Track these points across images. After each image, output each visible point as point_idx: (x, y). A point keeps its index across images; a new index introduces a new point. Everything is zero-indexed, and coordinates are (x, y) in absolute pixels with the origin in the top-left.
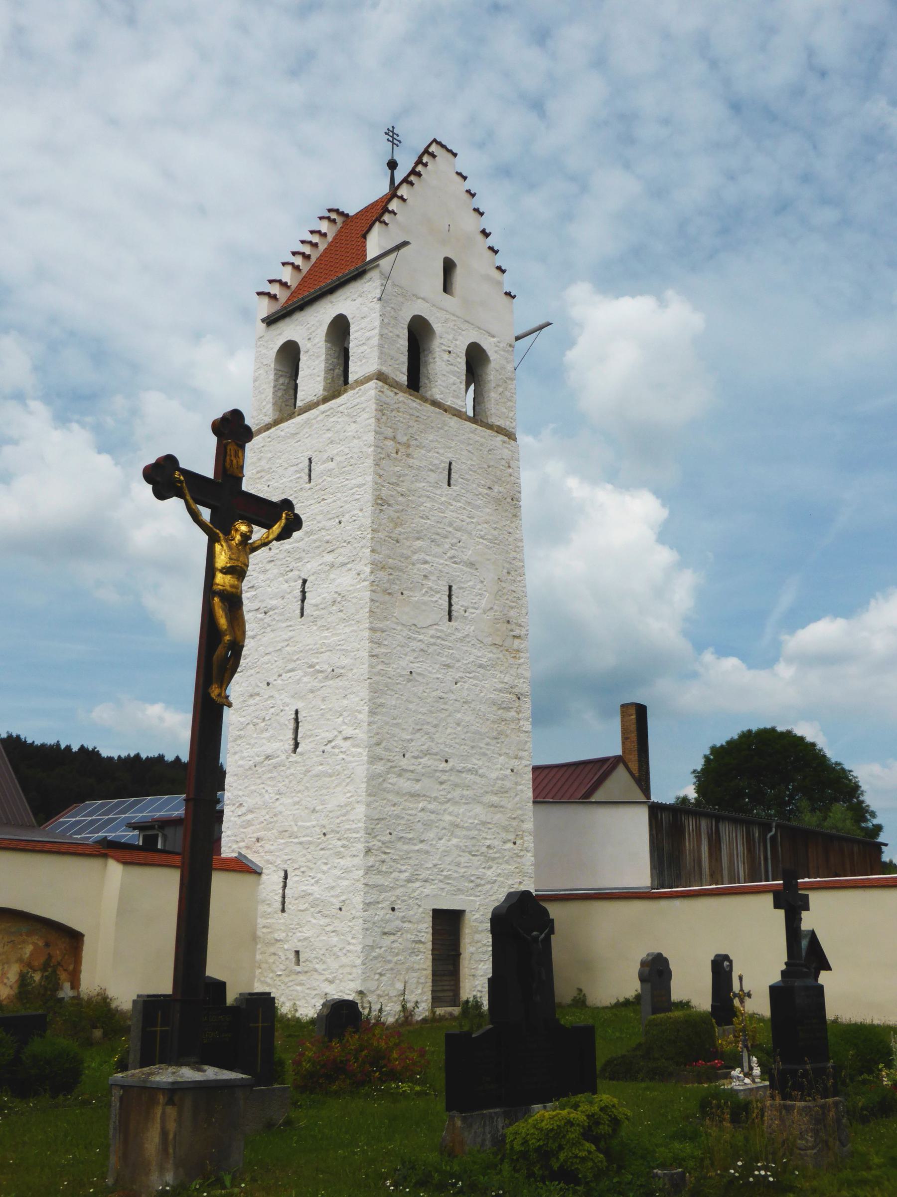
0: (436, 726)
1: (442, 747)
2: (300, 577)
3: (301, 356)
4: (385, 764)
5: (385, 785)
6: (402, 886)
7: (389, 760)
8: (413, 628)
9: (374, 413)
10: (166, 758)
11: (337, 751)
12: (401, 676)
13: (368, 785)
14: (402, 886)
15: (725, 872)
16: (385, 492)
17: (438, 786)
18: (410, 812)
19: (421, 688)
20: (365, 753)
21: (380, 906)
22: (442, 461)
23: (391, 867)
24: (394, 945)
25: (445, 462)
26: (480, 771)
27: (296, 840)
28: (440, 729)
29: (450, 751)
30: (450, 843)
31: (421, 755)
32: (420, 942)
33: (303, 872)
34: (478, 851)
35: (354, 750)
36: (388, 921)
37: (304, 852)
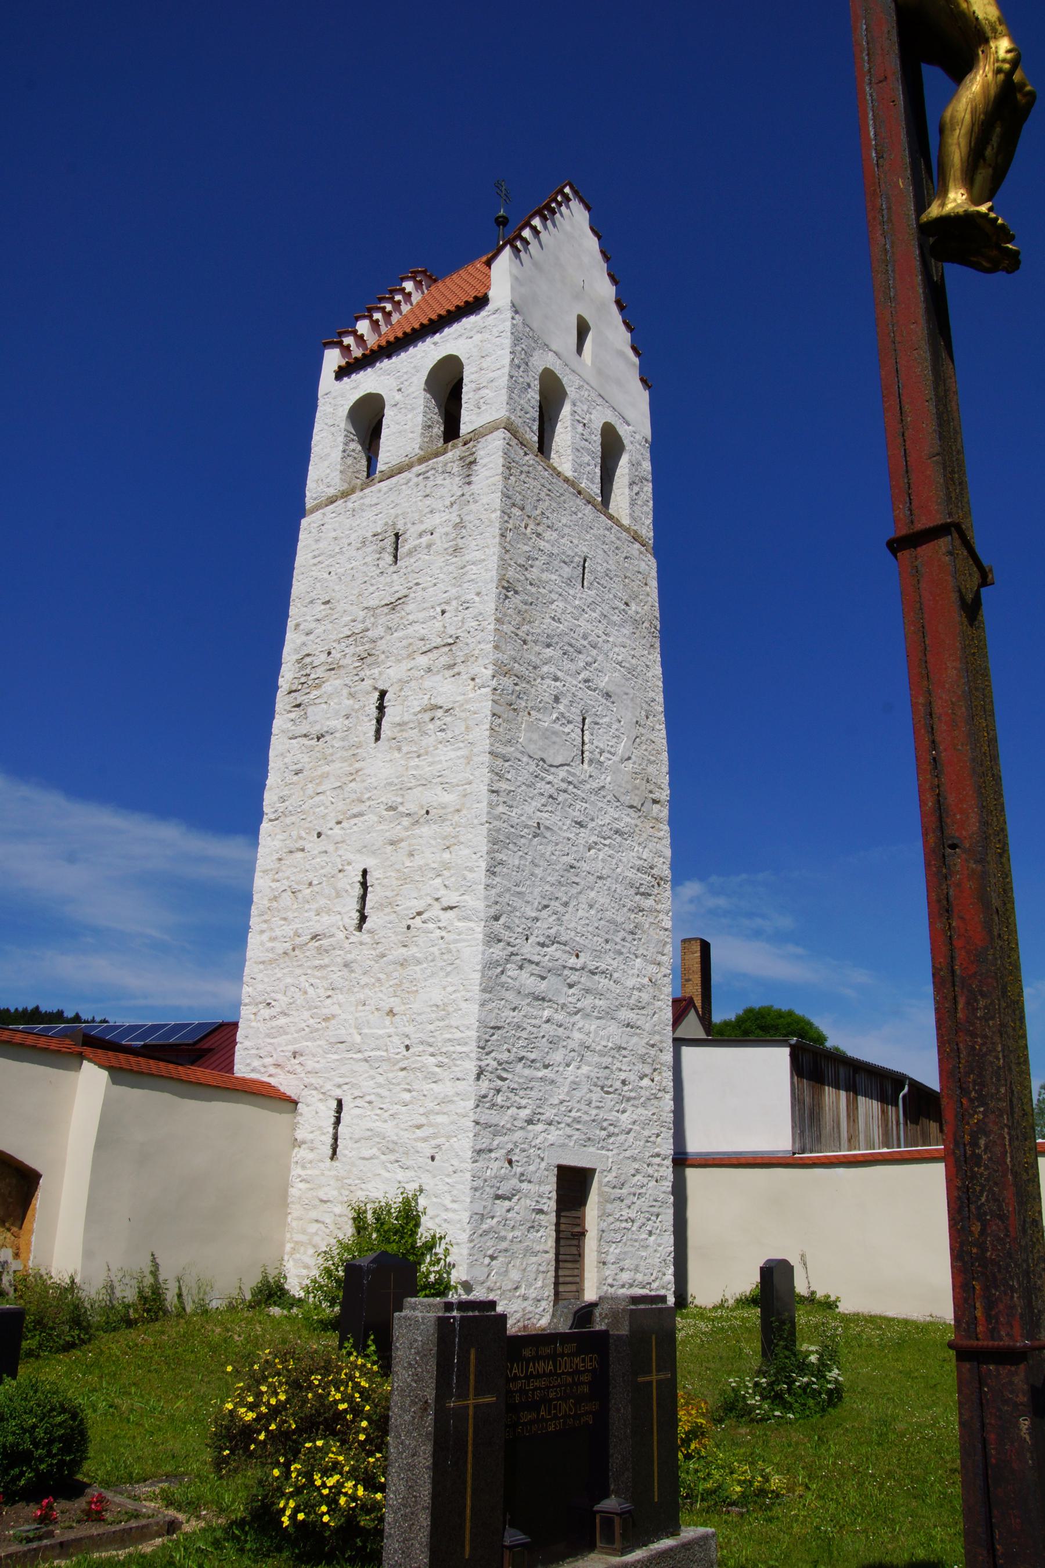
0: (566, 904)
1: (573, 934)
2: (376, 689)
3: (386, 411)
4: (504, 949)
5: (504, 978)
6: (521, 1128)
7: (509, 944)
8: (541, 763)
9: (501, 469)
10: (65, 1015)
11: (431, 926)
12: (526, 826)
13: (483, 976)
14: (521, 1128)
15: (862, 1137)
16: (511, 573)
17: (566, 989)
18: (533, 1021)
19: (550, 848)
20: (480, 929)
21: (493, 1155)
22: (576, 554)
23: (508, 1098)
24: (509, 1215)
25: (580, 556)
26: (615, 975)
27: (359, 1056)
28: (570, 909)
29: (582, 942)
30: (579, 1071)
31: (547, 942)
32: (541, 1211)
33: (370, 1102)
34: (611, 1086)
35: (460, 924)
36: (502, 1179)
37: (372, 1072)
